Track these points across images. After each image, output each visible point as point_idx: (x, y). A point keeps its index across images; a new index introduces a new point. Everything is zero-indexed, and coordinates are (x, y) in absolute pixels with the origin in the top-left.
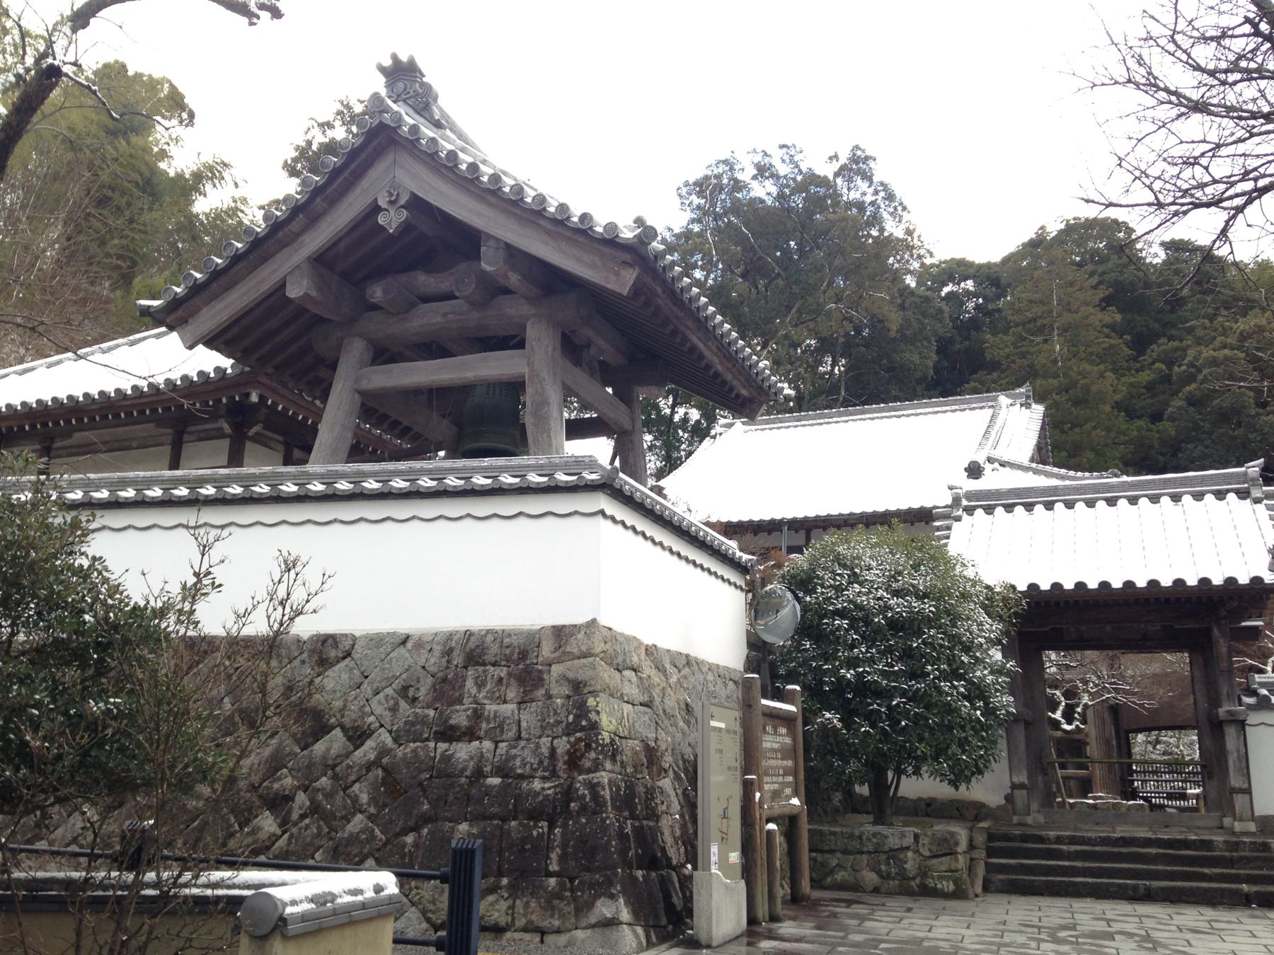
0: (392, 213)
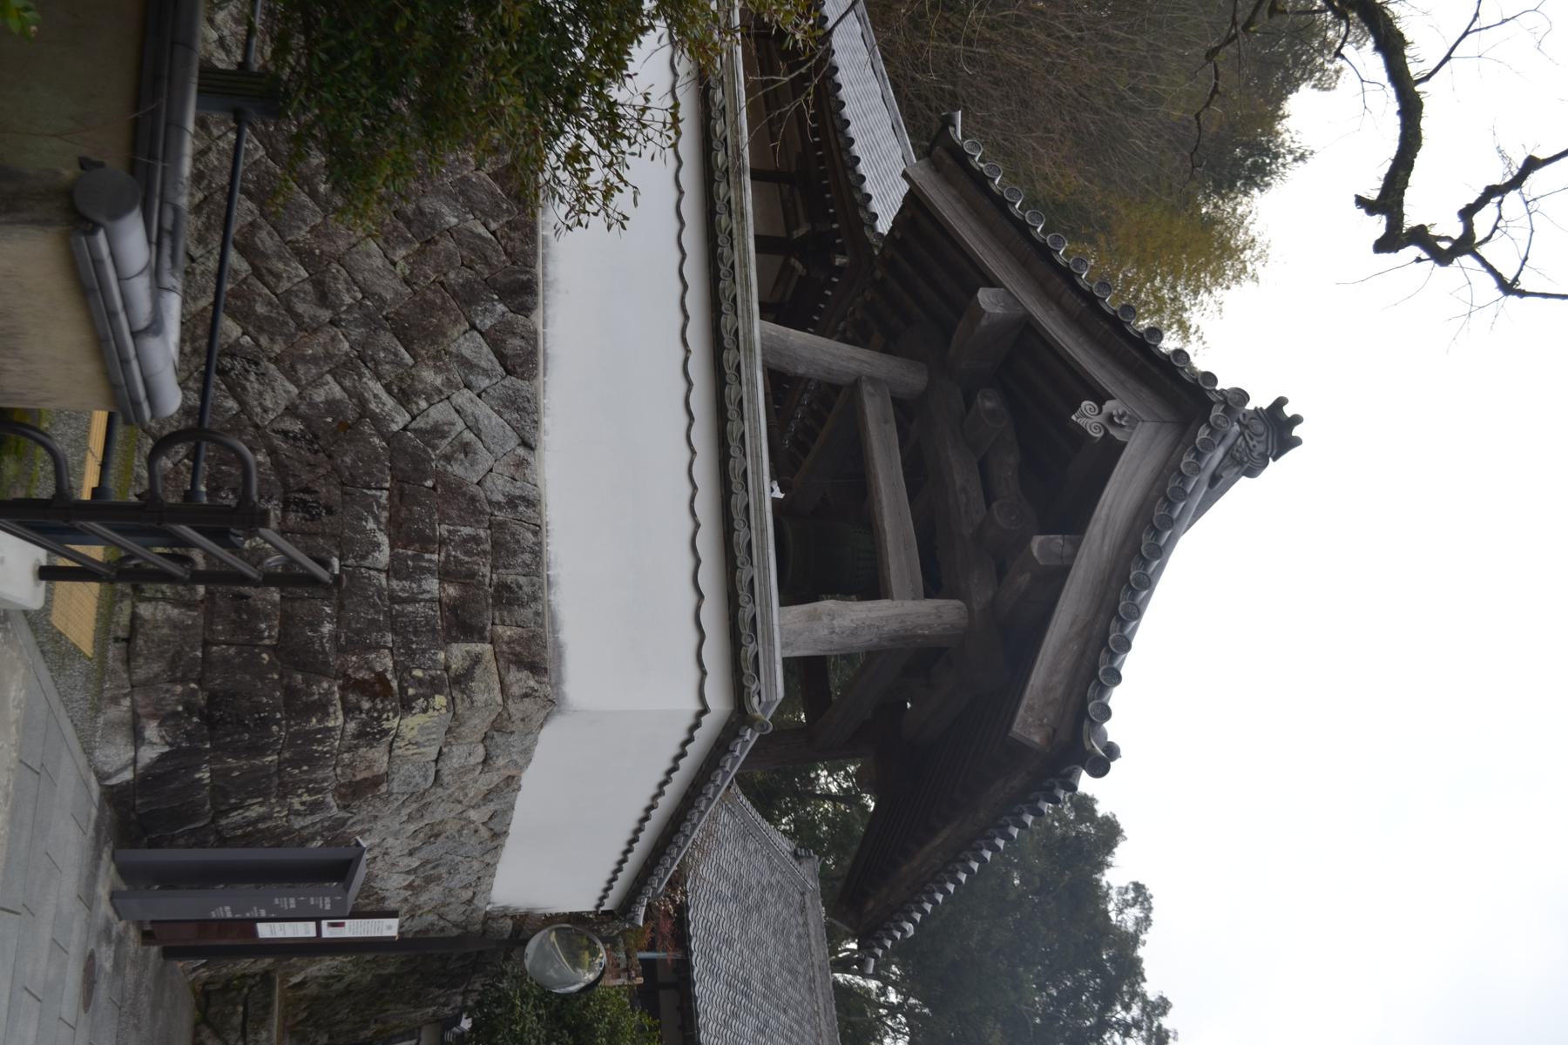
0: (1098, 419)
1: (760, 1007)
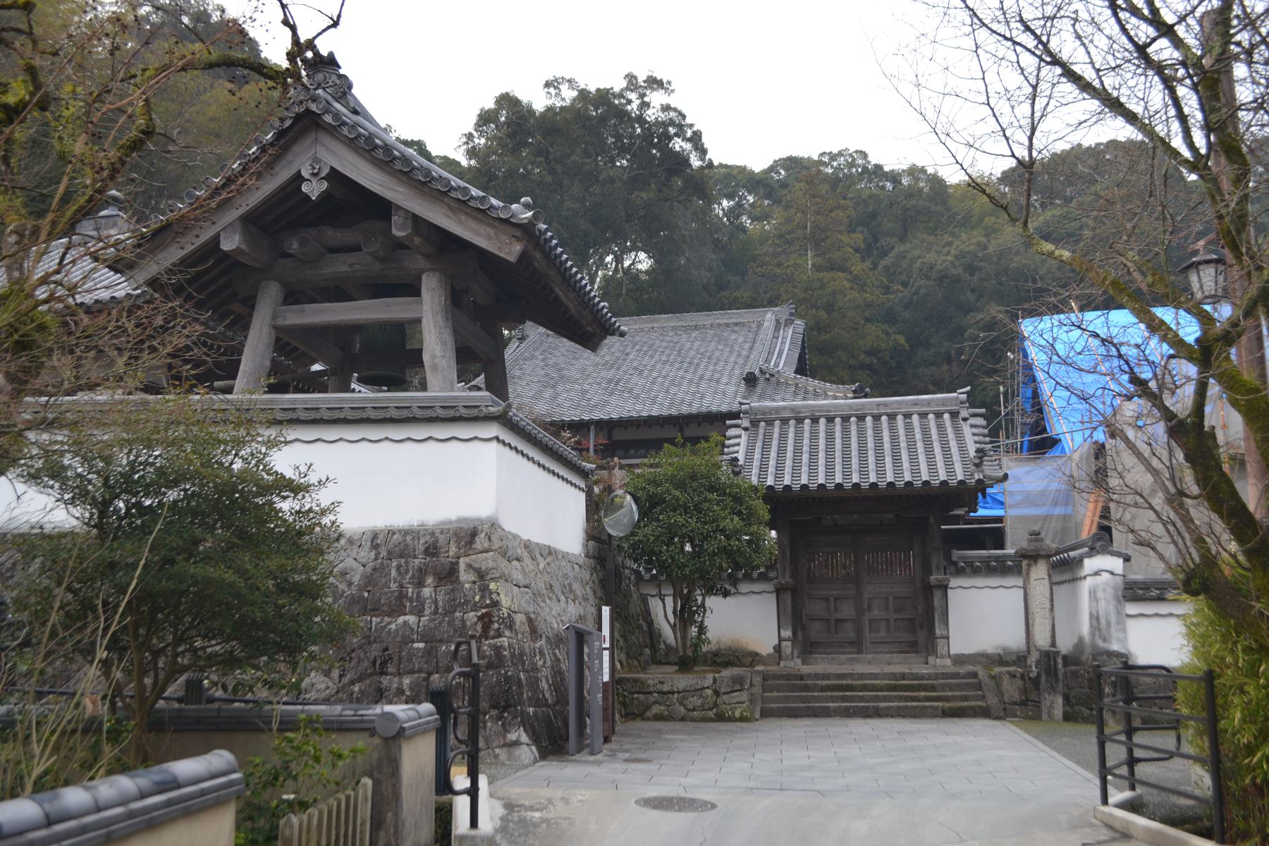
0: (314, 183)
1: (625, 372)
